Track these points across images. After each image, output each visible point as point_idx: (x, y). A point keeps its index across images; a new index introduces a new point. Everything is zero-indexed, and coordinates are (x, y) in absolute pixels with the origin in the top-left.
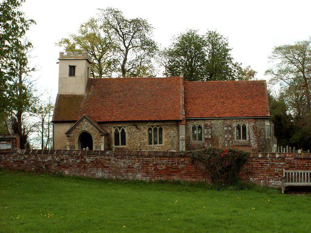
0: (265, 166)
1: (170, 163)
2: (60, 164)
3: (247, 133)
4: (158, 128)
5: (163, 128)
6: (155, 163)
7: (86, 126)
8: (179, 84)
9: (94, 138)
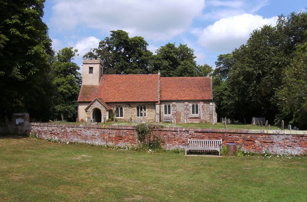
0: (176, 136)
1: (118, 133)
2: (52, 133)
3: (199, 110)
4: (143, 106)
5: (146, 107)
6: (108, 133)
7: (97, 105)
8: (157, 79)
9: (102, 112)
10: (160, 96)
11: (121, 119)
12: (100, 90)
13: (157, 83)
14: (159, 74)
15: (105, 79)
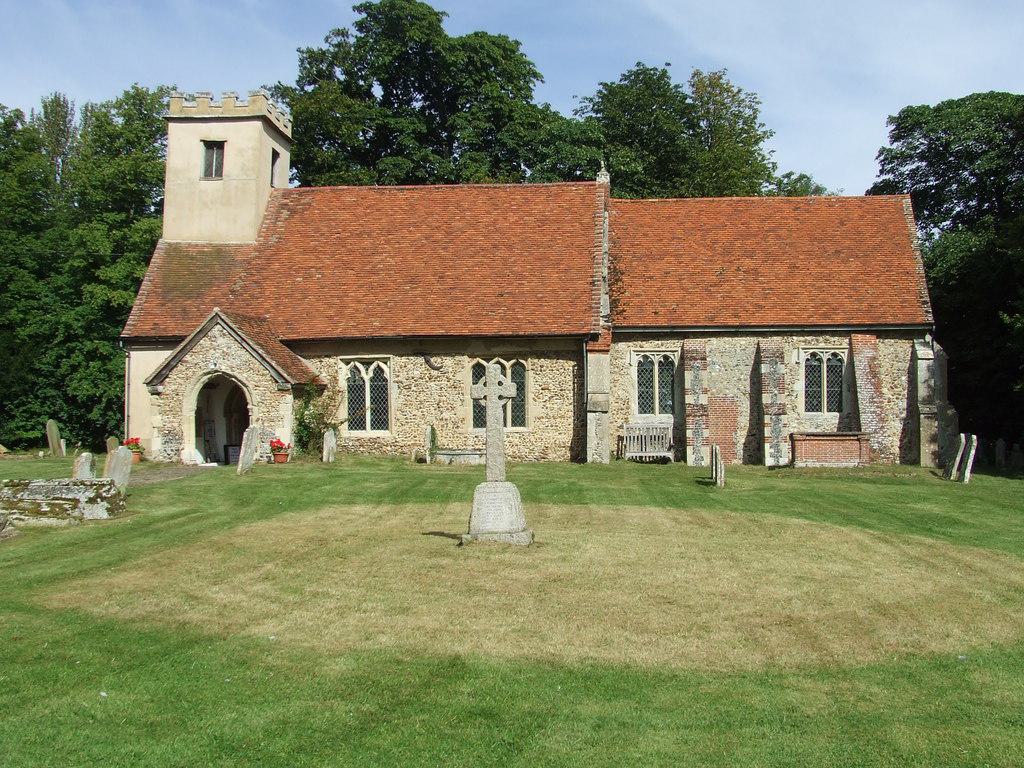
10: (614, 303)
11: (374, 441)
12: (260, 269)
13: (591, 227)
14: (603, 178)
15: (293, 212)
